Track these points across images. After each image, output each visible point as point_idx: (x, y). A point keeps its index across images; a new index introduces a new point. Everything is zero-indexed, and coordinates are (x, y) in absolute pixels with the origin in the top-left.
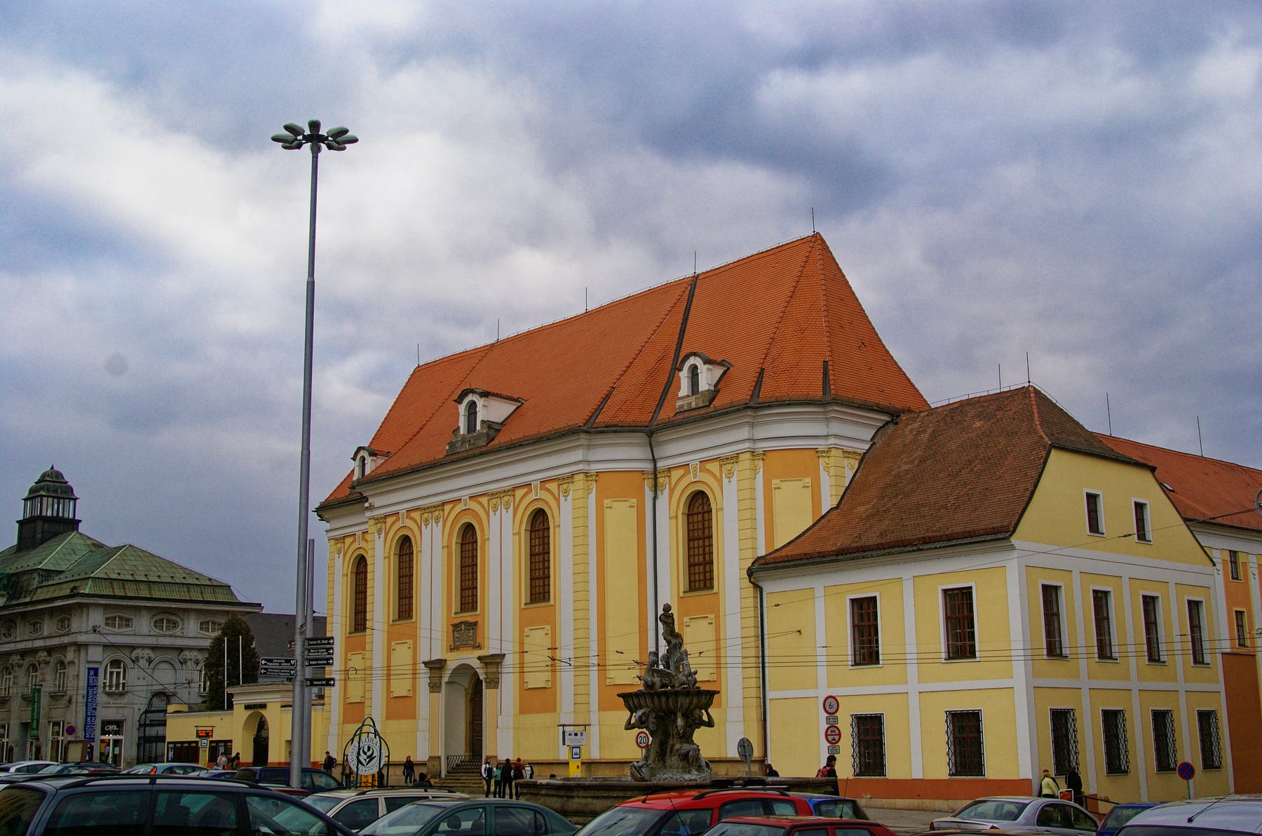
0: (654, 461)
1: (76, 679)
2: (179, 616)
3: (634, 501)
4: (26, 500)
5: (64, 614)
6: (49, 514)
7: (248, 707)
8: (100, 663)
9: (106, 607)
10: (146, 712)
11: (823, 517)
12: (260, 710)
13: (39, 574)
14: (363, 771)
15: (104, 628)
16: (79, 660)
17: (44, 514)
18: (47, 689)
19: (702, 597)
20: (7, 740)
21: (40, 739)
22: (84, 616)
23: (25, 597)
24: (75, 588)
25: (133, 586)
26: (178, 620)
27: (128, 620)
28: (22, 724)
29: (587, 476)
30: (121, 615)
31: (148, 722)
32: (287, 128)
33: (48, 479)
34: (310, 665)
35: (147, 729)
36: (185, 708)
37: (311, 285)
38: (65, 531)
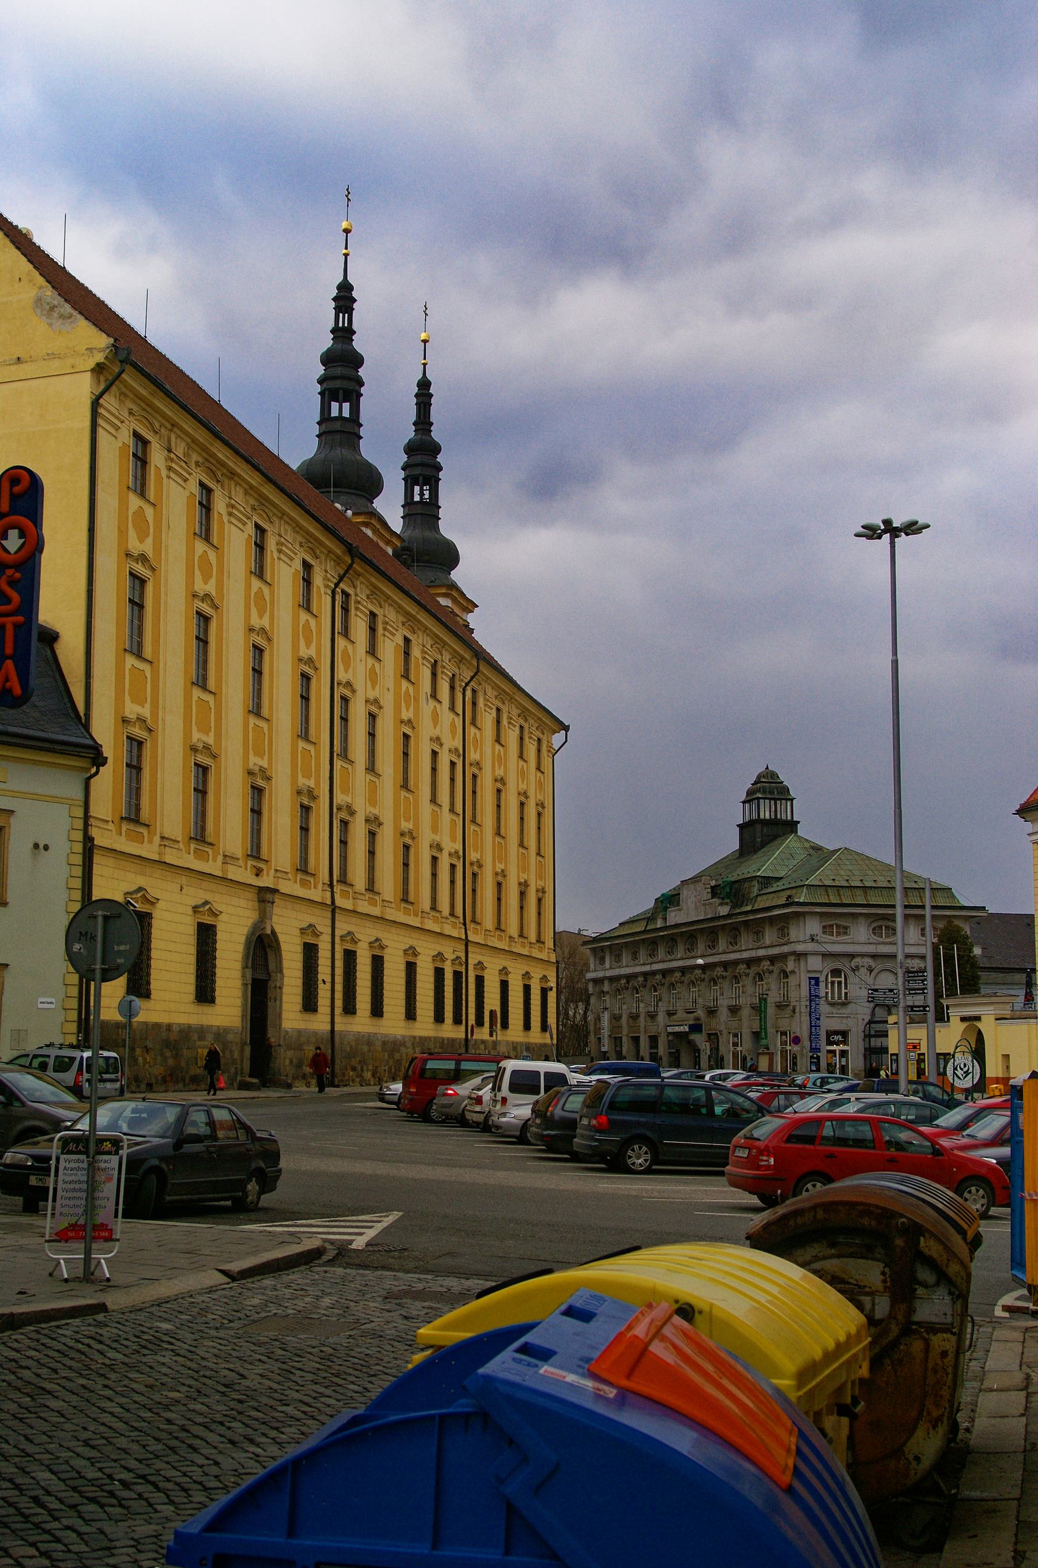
4: (744, 802)
5: (782, 923)
6: (767, 816)
7: (963, 1019)
8: (821, 972)
9: (822, 915)
10: (870, 1022)
12: (975, 1023)
14: (958, 1083)
15: (822, 937)
17: (762, 816)
18: (773, 1000)
22: (801, 924)
24: (789, 897)
25: (848, 893)
27: (846, 928)
31: (872, 1033)
32: (863, 527)
34: (910, 994)
35: (872, 1040)
37: (895, 663)
38: (784, 834)
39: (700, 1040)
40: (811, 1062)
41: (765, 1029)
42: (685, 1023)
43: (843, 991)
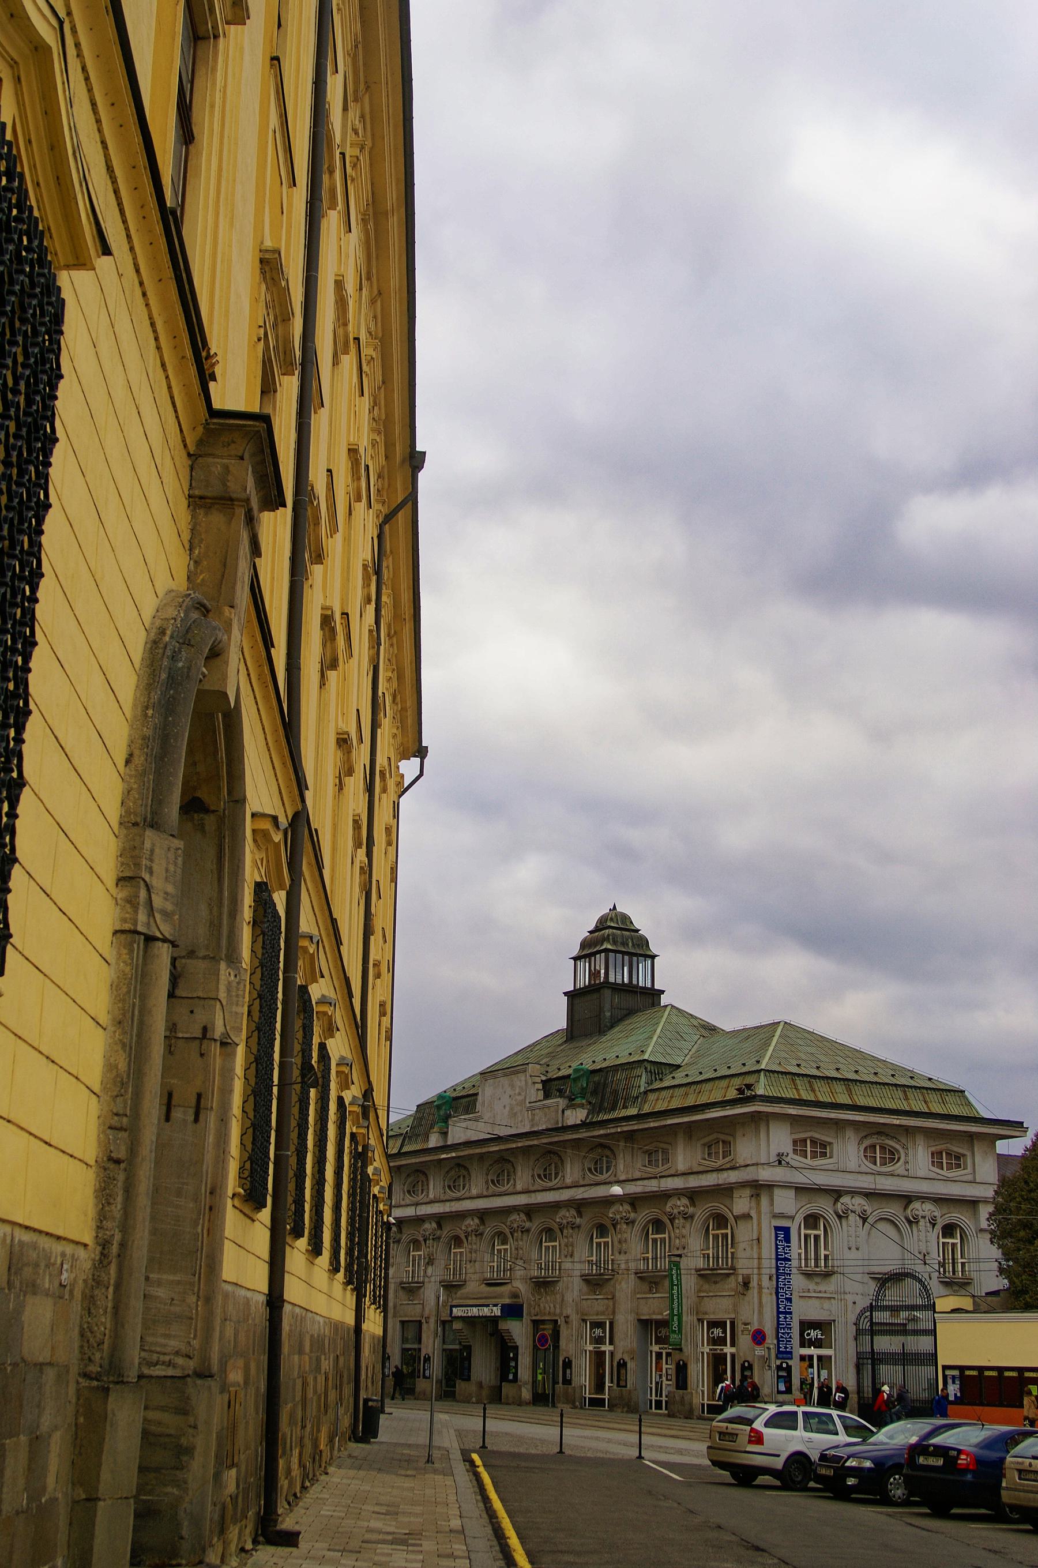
1: (755, 1247)
2: (899, 1141)
4: (575, 959)
8: (792, 1218)
10: (872, 1308)
13: (646, 1069)
16: (759, 1213)
17: (612, 979)
20: (733, 1350)
21: (685, 1349)
22: (763, 1135)
23: (625, 1107)
26: (897, 1147)
27: (824, 1145)
28: (639, 1320)
30: (817, 1136)
33: (612, 925)
36: (967, 1303)
39: (519, 1331)
40: (779, 1377)
41: (680, 1316)
42: (494, 1301)
43: (823, 1252)
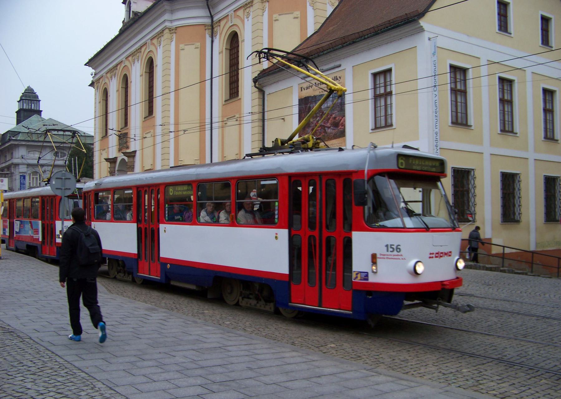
0: (212, 17)
3: (198, 44)
11: (308, 39)
19: (233, 104)
29: (170, 30)
